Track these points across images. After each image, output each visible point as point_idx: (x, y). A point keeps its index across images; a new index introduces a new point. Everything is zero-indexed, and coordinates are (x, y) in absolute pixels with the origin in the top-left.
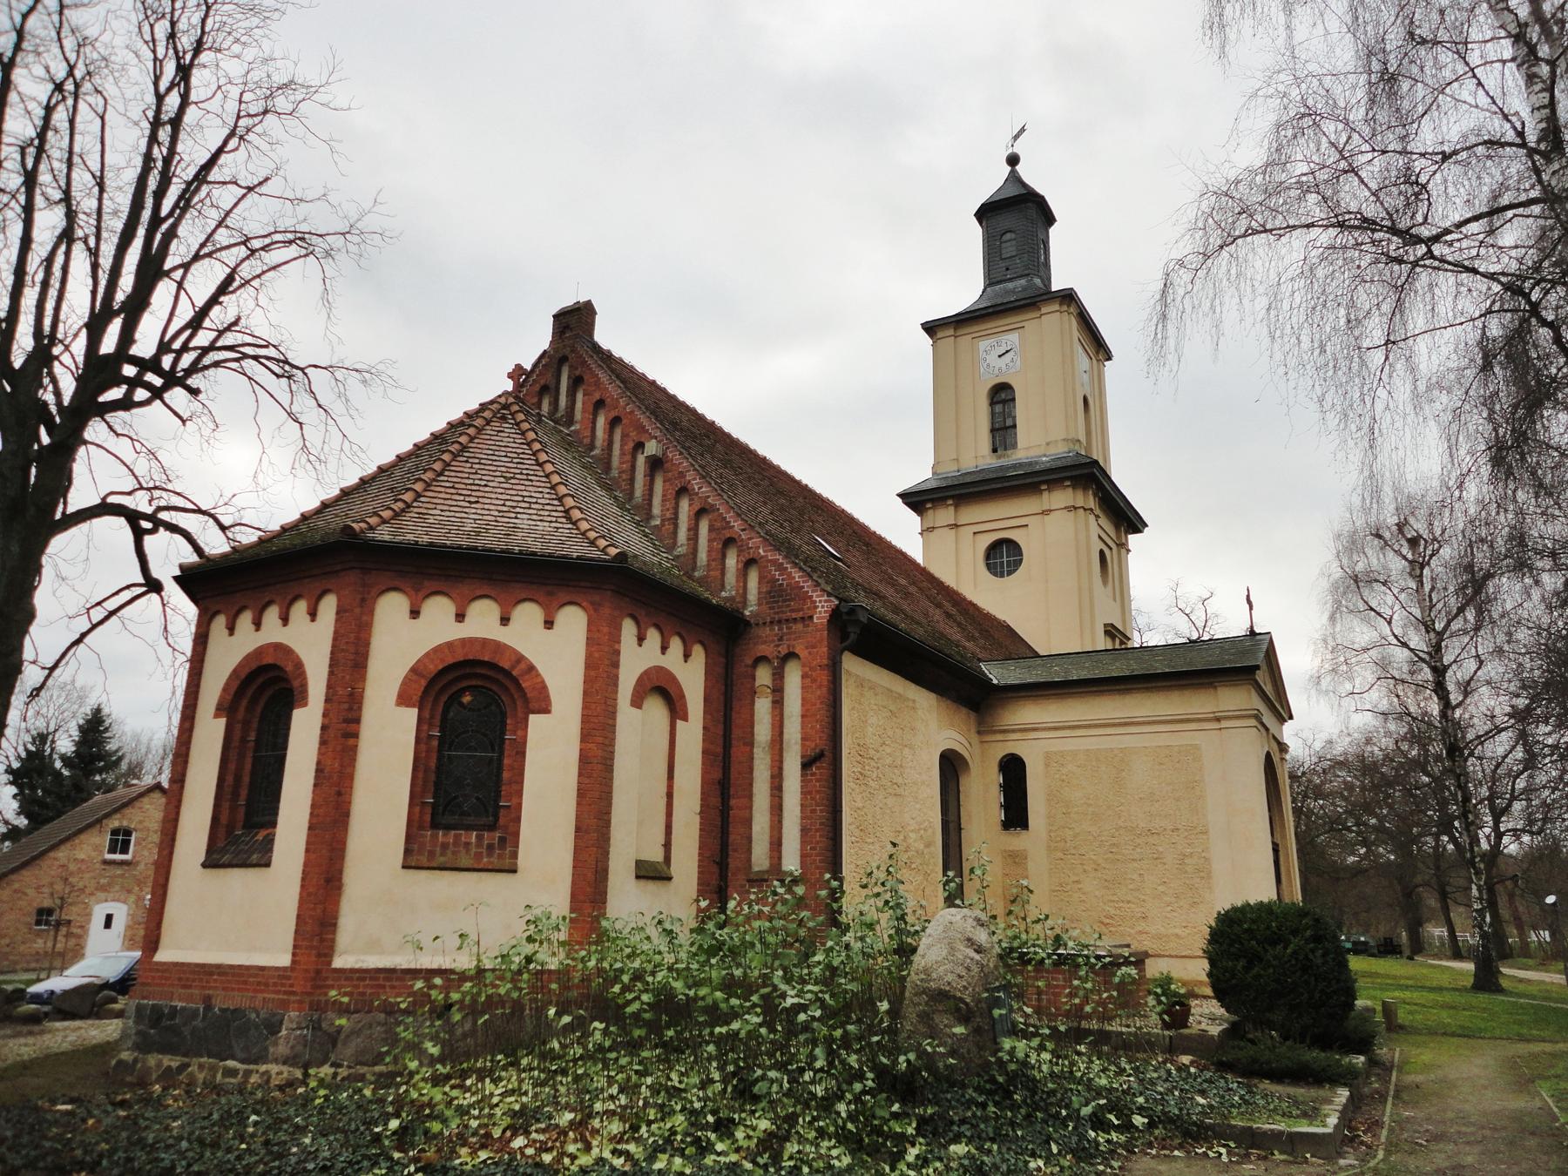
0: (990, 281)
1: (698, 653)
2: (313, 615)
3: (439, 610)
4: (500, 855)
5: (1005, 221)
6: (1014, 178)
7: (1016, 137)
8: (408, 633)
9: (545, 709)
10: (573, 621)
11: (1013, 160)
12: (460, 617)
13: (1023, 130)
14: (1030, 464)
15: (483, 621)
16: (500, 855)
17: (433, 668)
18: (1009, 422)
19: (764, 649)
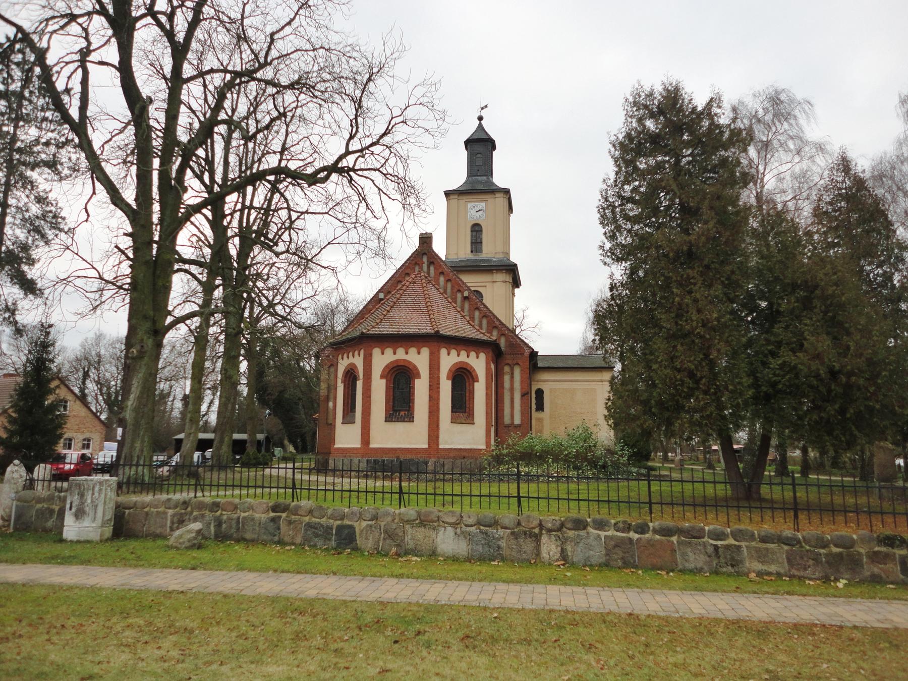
0: (471, 173)
1: (482, 356)
2: (359, 355)
3: (389, 351)
4: (410, 418)
5: (478, 148)
6: (480, 127)
7: (483, 108)
8: (382, 359)
9: (419, 376)
10: (425, 352)
11: (480, 118)
12: (395, 353)
13: (486, 106)
14: (488, 261)
15: (401, 354)
16: (410, 418)
17: (391, 367)
18: (474, 233)
19: (508, 361)
